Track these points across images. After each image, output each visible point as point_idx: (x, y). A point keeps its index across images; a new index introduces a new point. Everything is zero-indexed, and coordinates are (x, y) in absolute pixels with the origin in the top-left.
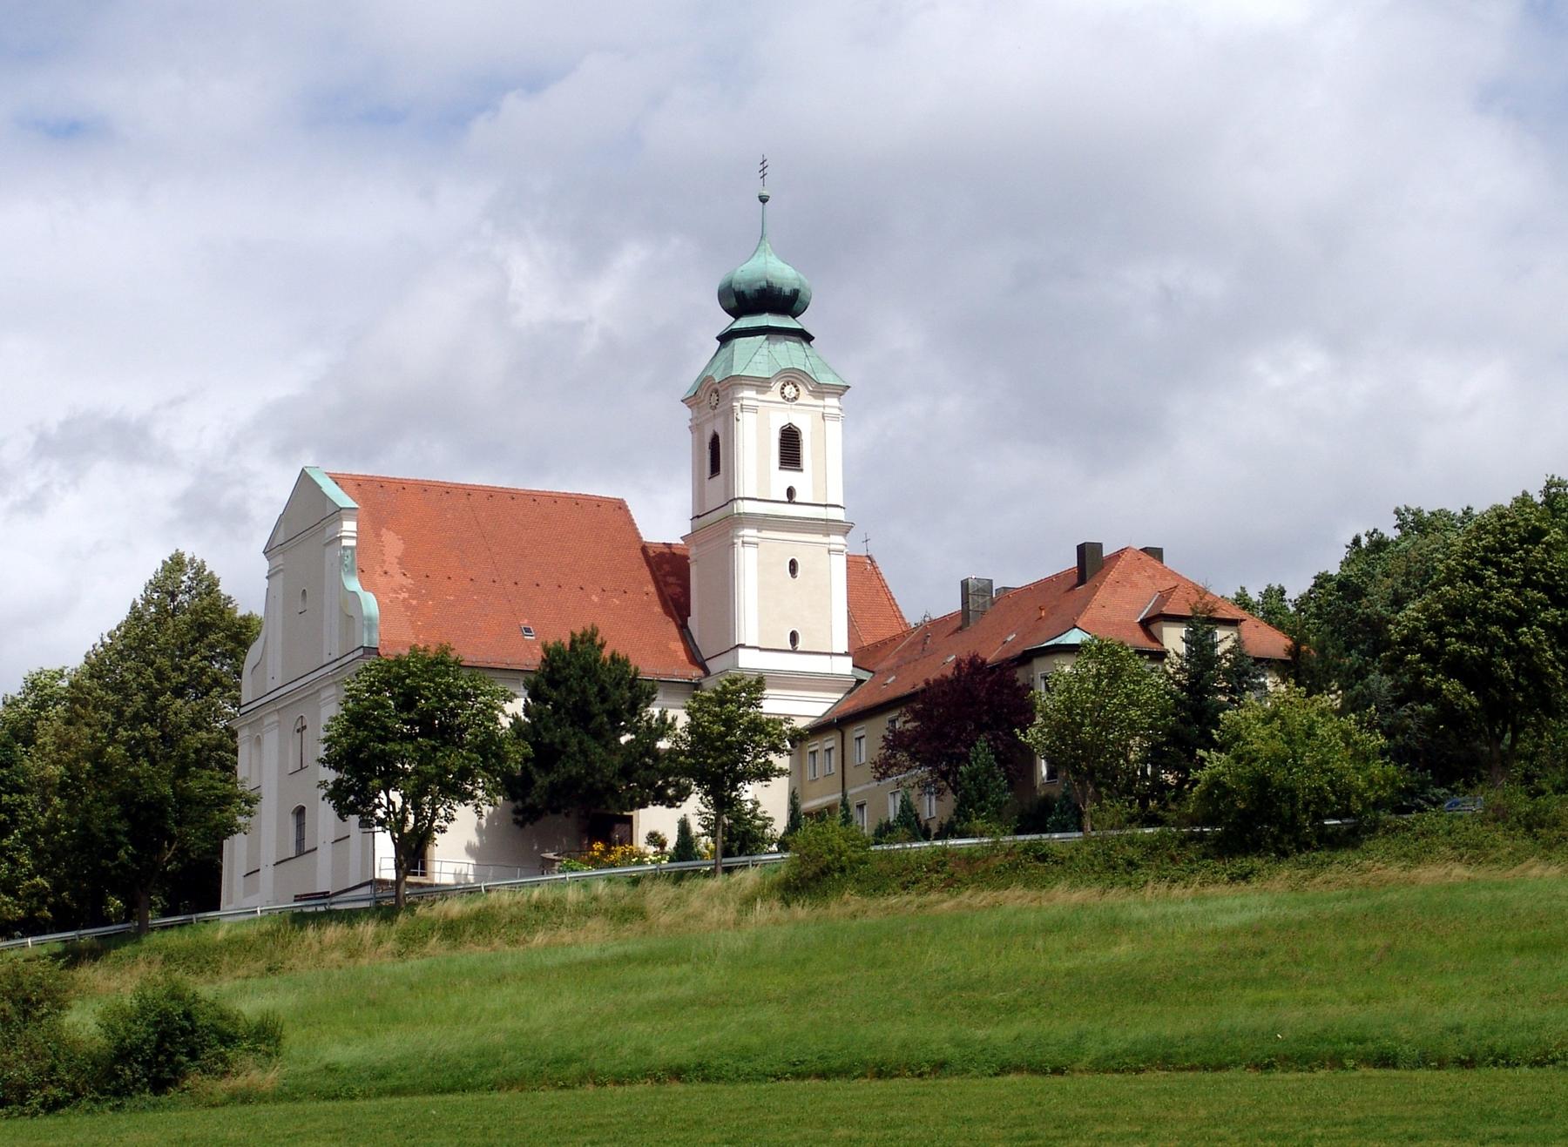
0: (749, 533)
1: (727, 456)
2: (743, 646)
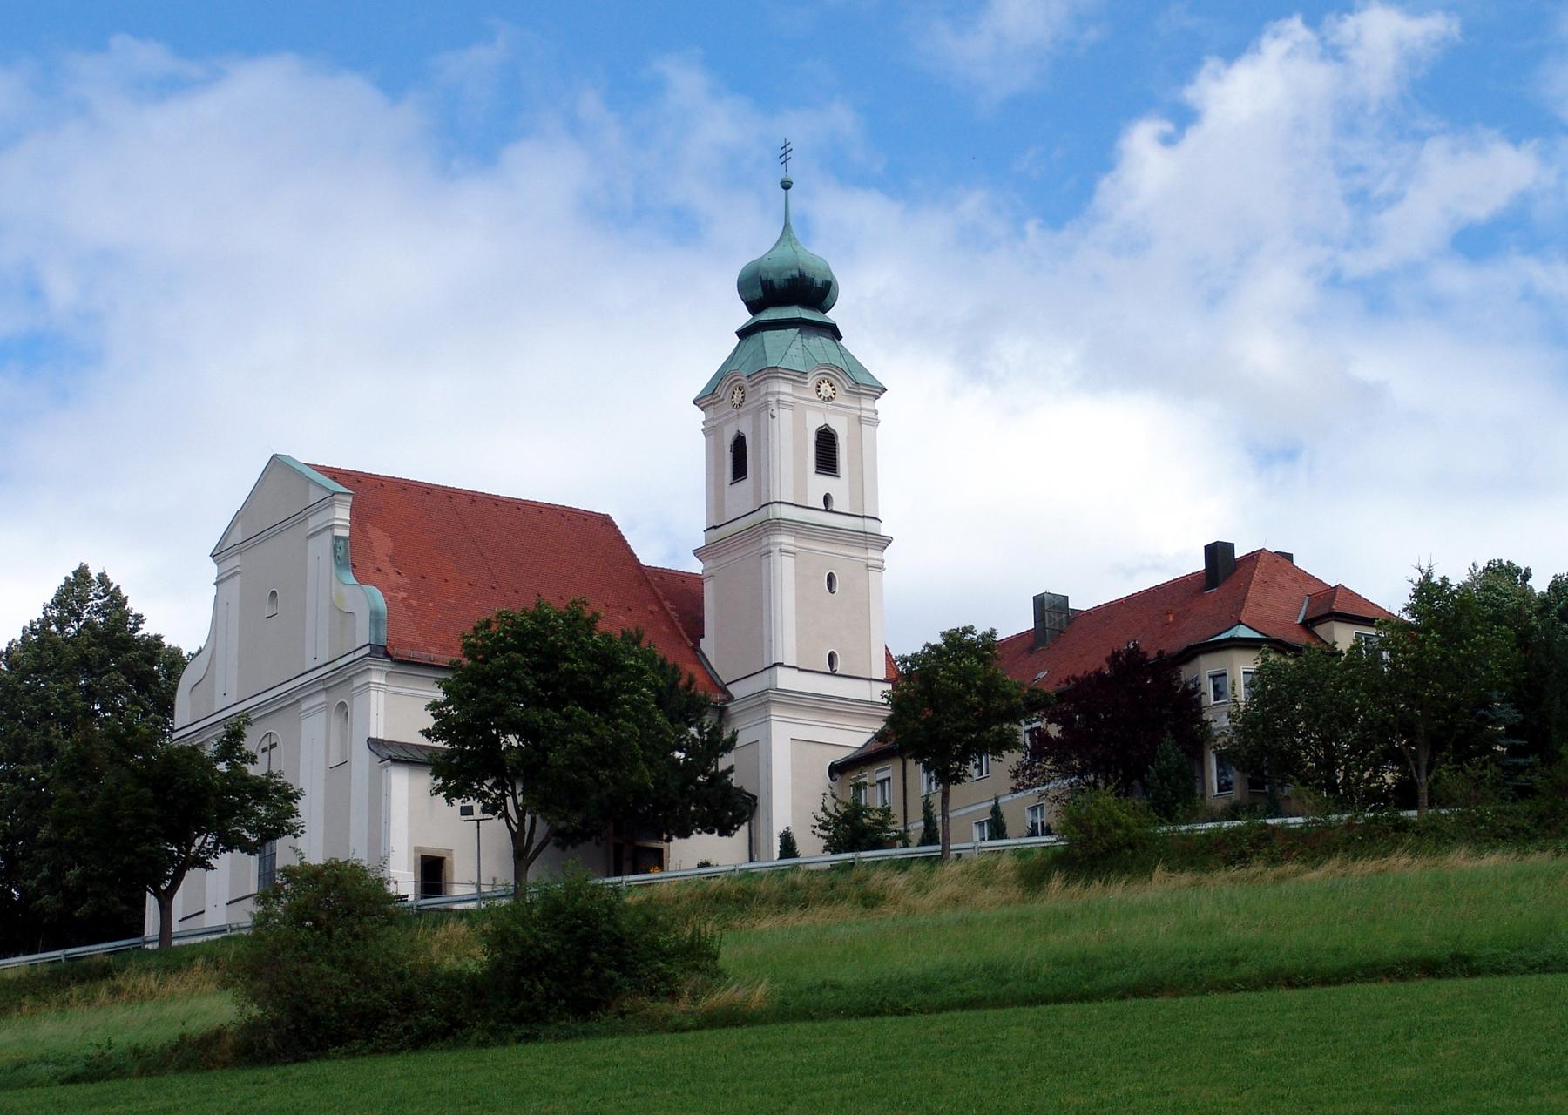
0: (787, 540)
1: (758, 458)
2: (781, 665)
